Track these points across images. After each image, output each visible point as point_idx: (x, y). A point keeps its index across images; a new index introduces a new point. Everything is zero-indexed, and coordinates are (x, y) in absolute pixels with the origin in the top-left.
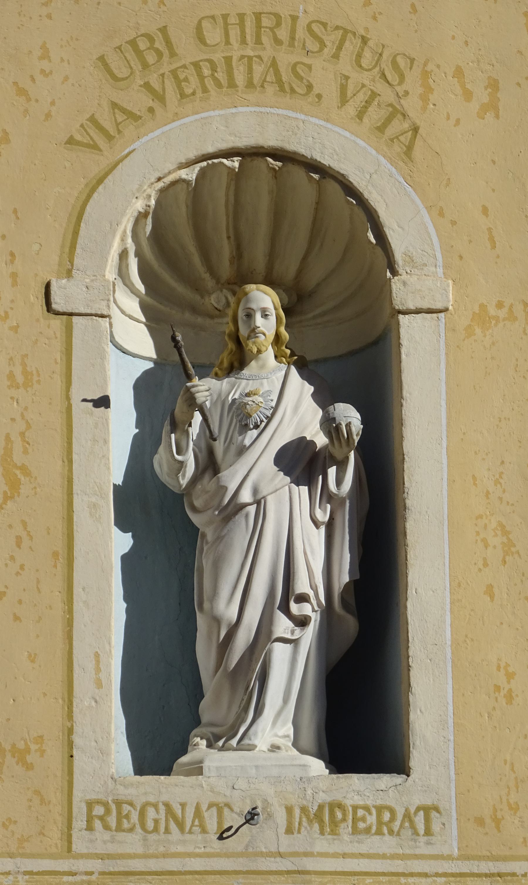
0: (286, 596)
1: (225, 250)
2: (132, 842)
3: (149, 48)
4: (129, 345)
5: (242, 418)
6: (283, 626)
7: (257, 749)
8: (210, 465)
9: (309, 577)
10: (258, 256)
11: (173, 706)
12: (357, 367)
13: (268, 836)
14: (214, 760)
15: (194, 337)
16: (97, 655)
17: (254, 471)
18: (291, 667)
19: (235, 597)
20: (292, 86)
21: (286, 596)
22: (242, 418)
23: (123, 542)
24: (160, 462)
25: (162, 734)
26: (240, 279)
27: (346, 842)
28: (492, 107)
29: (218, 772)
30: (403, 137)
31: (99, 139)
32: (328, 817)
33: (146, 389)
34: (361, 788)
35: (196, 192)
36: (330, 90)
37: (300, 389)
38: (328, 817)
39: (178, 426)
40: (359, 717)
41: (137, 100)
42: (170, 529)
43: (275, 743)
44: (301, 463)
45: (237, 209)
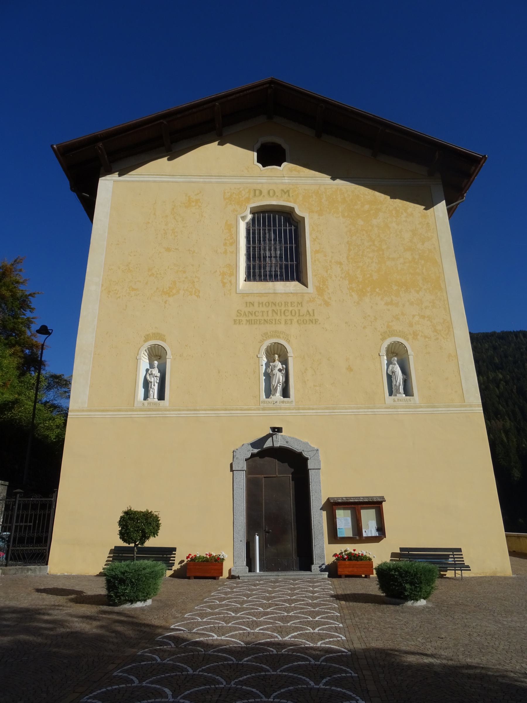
0: (279, 382)
1: (273, 352)
2: (266, 405)
3: (266, 334)
4: (265, 360)
5: (275, 366)
6: (279, 385)
7: (281, 434)
8: (272, 371)
9: (281, 381)
10: (276, 352)
11: (269, 392)
12: (285, 362)
13: (278, 404)
14: (273, 397)
15: (270, 359)
16: (38, 590)
17: (276, 371)
18: (279, 389)
19: (274, 383)
20: (278, 337)
21: (279, 382)
22: (275, 366)
23: (264, 378)
24: (267, 371)
25: (268, 395)
26: (274, 354)
27: (284, 404)
28: (296, 338)
29: (273, 398)
30: (289, 342)
31: (262, 342)
32: (283, 402)
33: (266, 364)
34: (286, 399)
35: (270, 347)
36: (282, 337)
37: (280, 364)
38: (283, 402)
39: (269, 367)
40: (285, 393)
41: (265, 338)
42: (268, 376)
43: (278, 395)
44: (280, 370)
45: (274, 348)
